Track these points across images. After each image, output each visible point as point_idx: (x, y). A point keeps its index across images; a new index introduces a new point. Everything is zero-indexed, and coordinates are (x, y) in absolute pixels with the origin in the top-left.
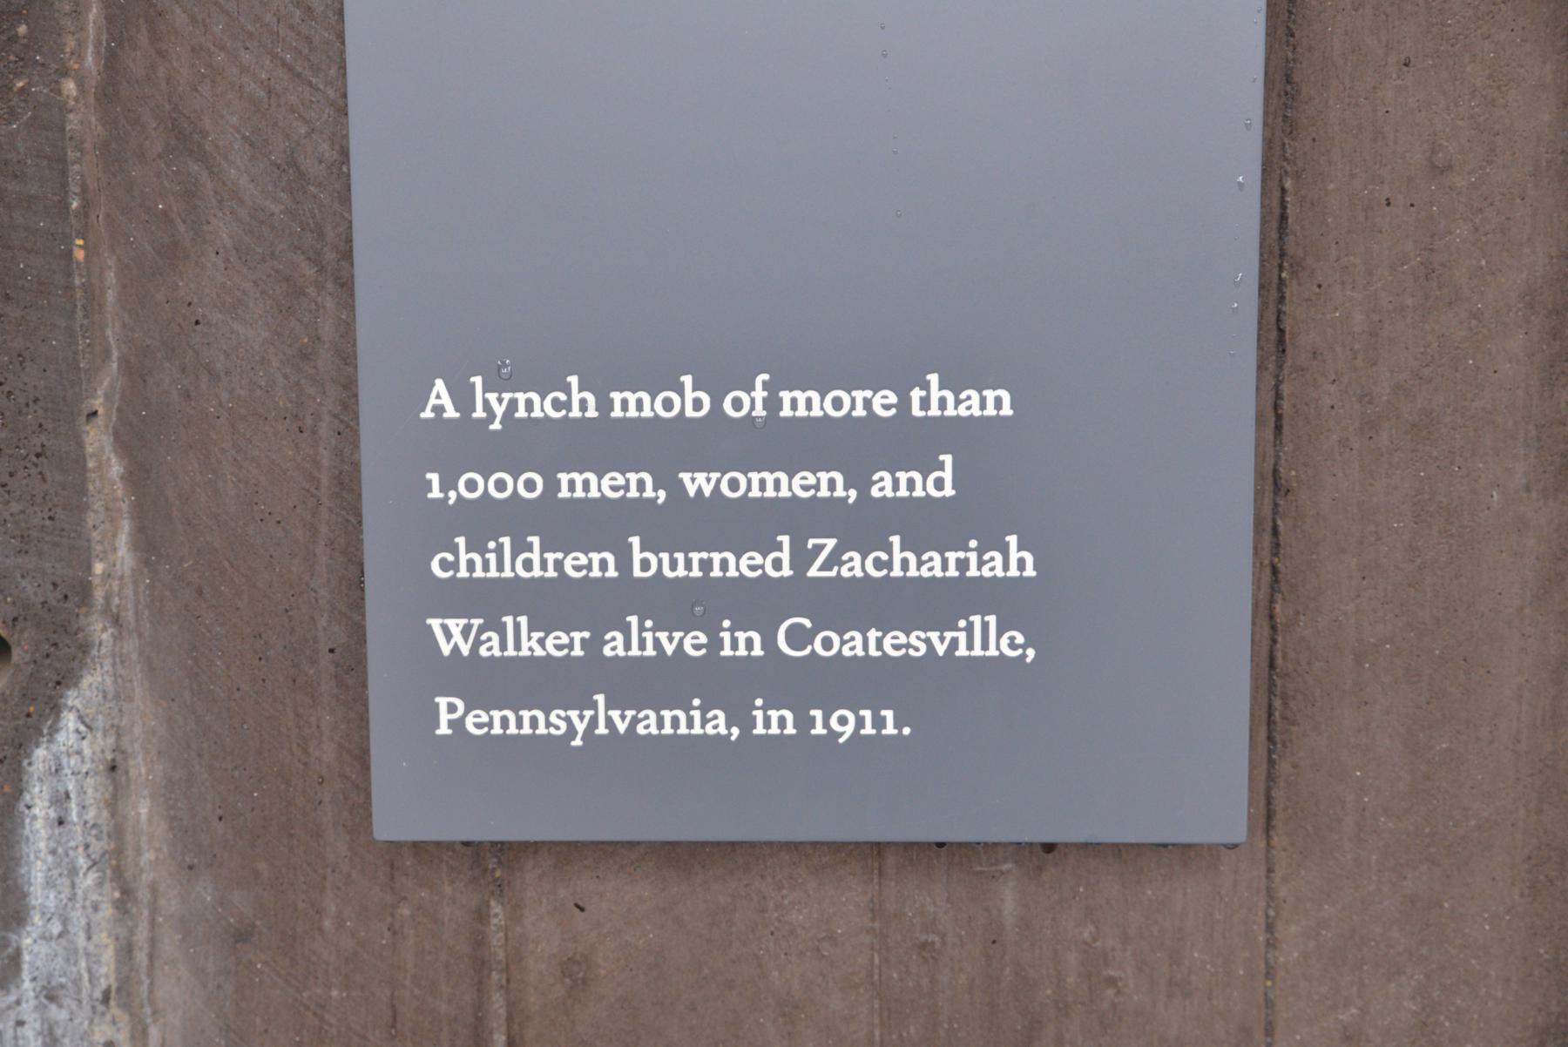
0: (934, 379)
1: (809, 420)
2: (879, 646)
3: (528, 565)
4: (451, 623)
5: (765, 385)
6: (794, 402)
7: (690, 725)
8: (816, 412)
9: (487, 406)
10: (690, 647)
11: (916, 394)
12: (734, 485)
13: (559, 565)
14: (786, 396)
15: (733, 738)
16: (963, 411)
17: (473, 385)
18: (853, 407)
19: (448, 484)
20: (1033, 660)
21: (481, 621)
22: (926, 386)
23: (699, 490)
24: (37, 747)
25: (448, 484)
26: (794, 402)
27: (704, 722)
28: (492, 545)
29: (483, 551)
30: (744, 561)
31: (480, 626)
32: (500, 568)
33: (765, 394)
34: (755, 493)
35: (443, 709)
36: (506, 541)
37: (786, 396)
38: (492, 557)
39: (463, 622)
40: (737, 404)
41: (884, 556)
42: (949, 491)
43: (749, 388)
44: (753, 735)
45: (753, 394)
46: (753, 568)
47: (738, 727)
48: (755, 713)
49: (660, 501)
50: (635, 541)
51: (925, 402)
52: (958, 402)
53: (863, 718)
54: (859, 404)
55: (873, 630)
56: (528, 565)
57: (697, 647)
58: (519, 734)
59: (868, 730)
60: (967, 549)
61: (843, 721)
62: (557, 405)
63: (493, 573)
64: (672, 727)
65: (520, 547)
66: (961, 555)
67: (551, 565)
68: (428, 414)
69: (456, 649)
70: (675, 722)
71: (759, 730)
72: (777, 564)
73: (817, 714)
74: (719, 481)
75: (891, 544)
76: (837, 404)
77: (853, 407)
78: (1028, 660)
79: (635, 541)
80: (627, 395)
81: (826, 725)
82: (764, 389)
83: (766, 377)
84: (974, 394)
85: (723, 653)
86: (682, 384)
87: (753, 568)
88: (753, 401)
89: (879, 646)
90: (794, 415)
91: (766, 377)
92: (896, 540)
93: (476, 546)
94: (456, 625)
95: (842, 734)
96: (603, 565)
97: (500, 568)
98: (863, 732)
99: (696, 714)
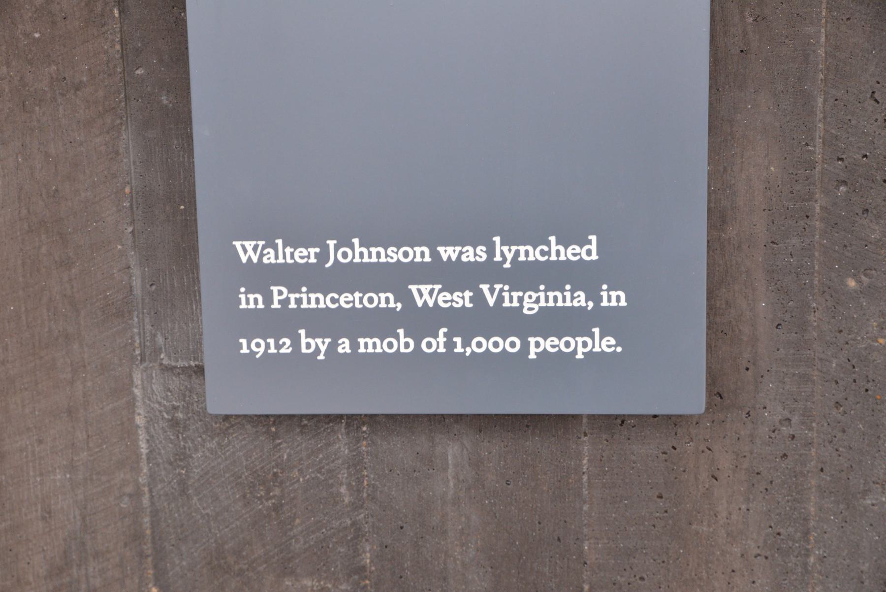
2: (292, 257)
4: (247, 244)
5: (445, 335)
7: (564, 301)
8: (322, 305)
15: (589, 308)
17: (494, 242)
19: (466, 344)
21: (263, 242)
23: (449, 257)
25: (466, 344)
27: (573, 298)
30: (569, 251)
31: (263, 245)
33: (445, 339)
35: (275, 293)
39: (253, 243)
40: (429, 345)
41: (546, 248)
42: (594, 257)
43: (436, 336)
45: (438, 339)
46: (574, 255)
47: (592, 301)
48: (240, 296)
50: (497, 240)
53: (269, 343)
55: (357, 293)
59: (273, 350)
60: (300, 292)
61: (258, 345)
62: (543, 253)
66: (297, 295)
69: (250, 259)
70: (556, 299)
71: (605, 303)
72: (589, 253)
73: (244, 341)
75: (353, 244)
79: (497, 240)
81: (249, 347)
83: (445, 330)
85: (242, 352)
87: (574, 255)
88: (438, 343)
89: (292, 257)
91: (445, 330)
92: (553, 239)
94: (249, 245)
95: (258, 353)
96: (423, 254)
98: (269, 351)
99: (568, 295)
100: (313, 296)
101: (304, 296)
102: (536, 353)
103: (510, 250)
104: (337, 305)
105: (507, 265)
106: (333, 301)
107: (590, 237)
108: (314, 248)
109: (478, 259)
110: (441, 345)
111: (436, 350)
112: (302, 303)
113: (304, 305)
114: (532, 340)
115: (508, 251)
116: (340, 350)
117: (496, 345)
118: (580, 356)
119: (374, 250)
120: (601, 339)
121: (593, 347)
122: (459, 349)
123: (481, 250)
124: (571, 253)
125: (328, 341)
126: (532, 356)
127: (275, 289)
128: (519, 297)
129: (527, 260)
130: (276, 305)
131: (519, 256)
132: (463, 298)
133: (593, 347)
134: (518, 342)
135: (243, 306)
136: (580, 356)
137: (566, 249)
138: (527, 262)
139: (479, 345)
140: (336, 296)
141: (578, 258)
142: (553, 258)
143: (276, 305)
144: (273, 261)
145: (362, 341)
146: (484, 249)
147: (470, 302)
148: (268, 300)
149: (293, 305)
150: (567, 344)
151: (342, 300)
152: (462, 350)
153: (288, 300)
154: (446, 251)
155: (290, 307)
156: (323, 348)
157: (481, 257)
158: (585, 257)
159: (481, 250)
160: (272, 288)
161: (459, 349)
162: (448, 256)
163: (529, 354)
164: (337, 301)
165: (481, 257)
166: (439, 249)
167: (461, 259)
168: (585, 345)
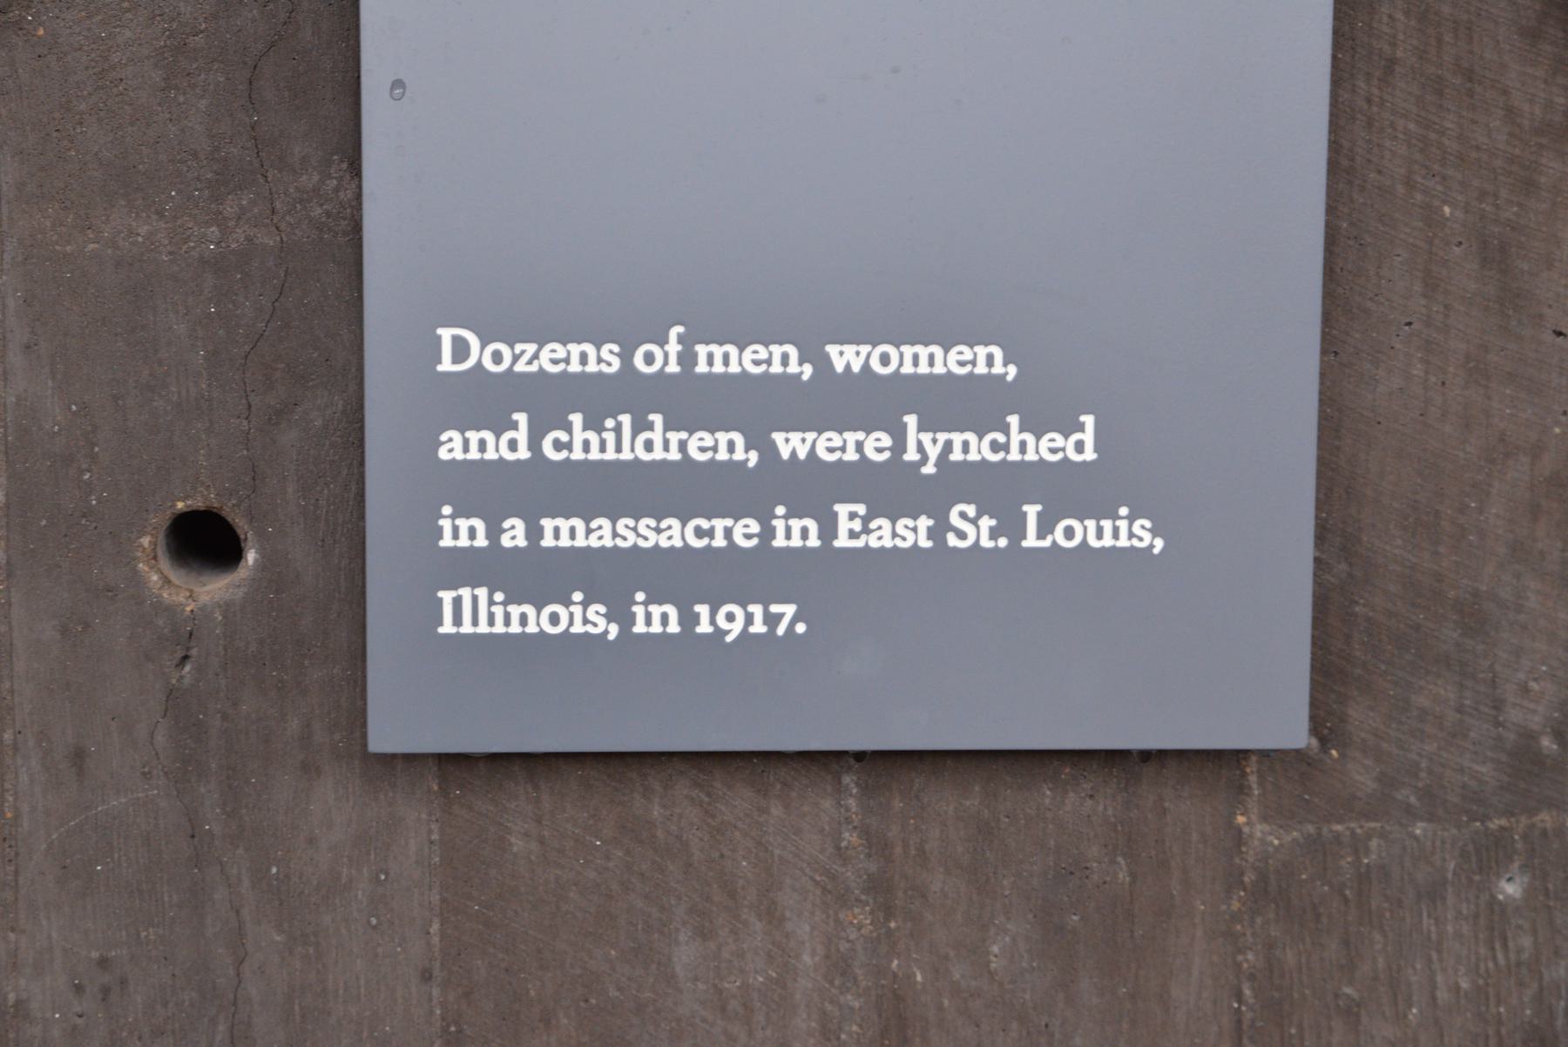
1: (726, 377)
3: (649, 446)
6: (710, 357)
9: (920, 448)
12: (885, 360)
13: (683, 446)
14: (702, 350)
17: (905, 425)
24: (205, 605)
26: (710, 357)
28: (610, 423)
29: (600, 429)
30: (1044, 443)
32: (619, 450)
33: (680, 348)
34: (908, 369)
36: (626, 419)
37: (702, 350)
38: (610, 437)
40: (649, 358)
41: (1001, 438)
42: (1089, 455)
43: (662, 342)
44: (1021, 547)
45: (667, 348)
46: (1053, 451)
48: (441, 522)
50: (911, 421)
52: (589, 531)
56: (649, 446)
57: (748, 537)
58: (523, 632)
59: (758, 627)
61: (730, 617)
63: (610, 455)
65: (641, 425)
67: (674, 446)
71: (640, 628)
72: (1080, 447)
75: (1008, 425)
79: (911, 421)
81: (713, 622)
83: (680, 329)
85: (441, 630)
87: (1053, 451)
88: (666, 355)
91: (680, 329)
92: (1014, 420)
93: (594, 424)
95: (728, 632)
97: (619, 450)
98: (752, 630)
103: (935, 441)
105: (929, 469)
107: (1083, 418)
108: (855, 431)
110: (673, 359)
111: (567, 630)
115: (931, 444)
119: (474, 437)
124: (1047, 448)
127: (842, 510)
131: (951, 451)
132: (915, 530)
135: (447, 541)
137: (1038, 439)
138: (965, 464)
141: (1059, 456)
142: (1014, 456)
144: (459, 455)
147: (929, 538)
154: (787, 440)
158: (1074, 457)
160: (440, 331)
162: (791, 449)
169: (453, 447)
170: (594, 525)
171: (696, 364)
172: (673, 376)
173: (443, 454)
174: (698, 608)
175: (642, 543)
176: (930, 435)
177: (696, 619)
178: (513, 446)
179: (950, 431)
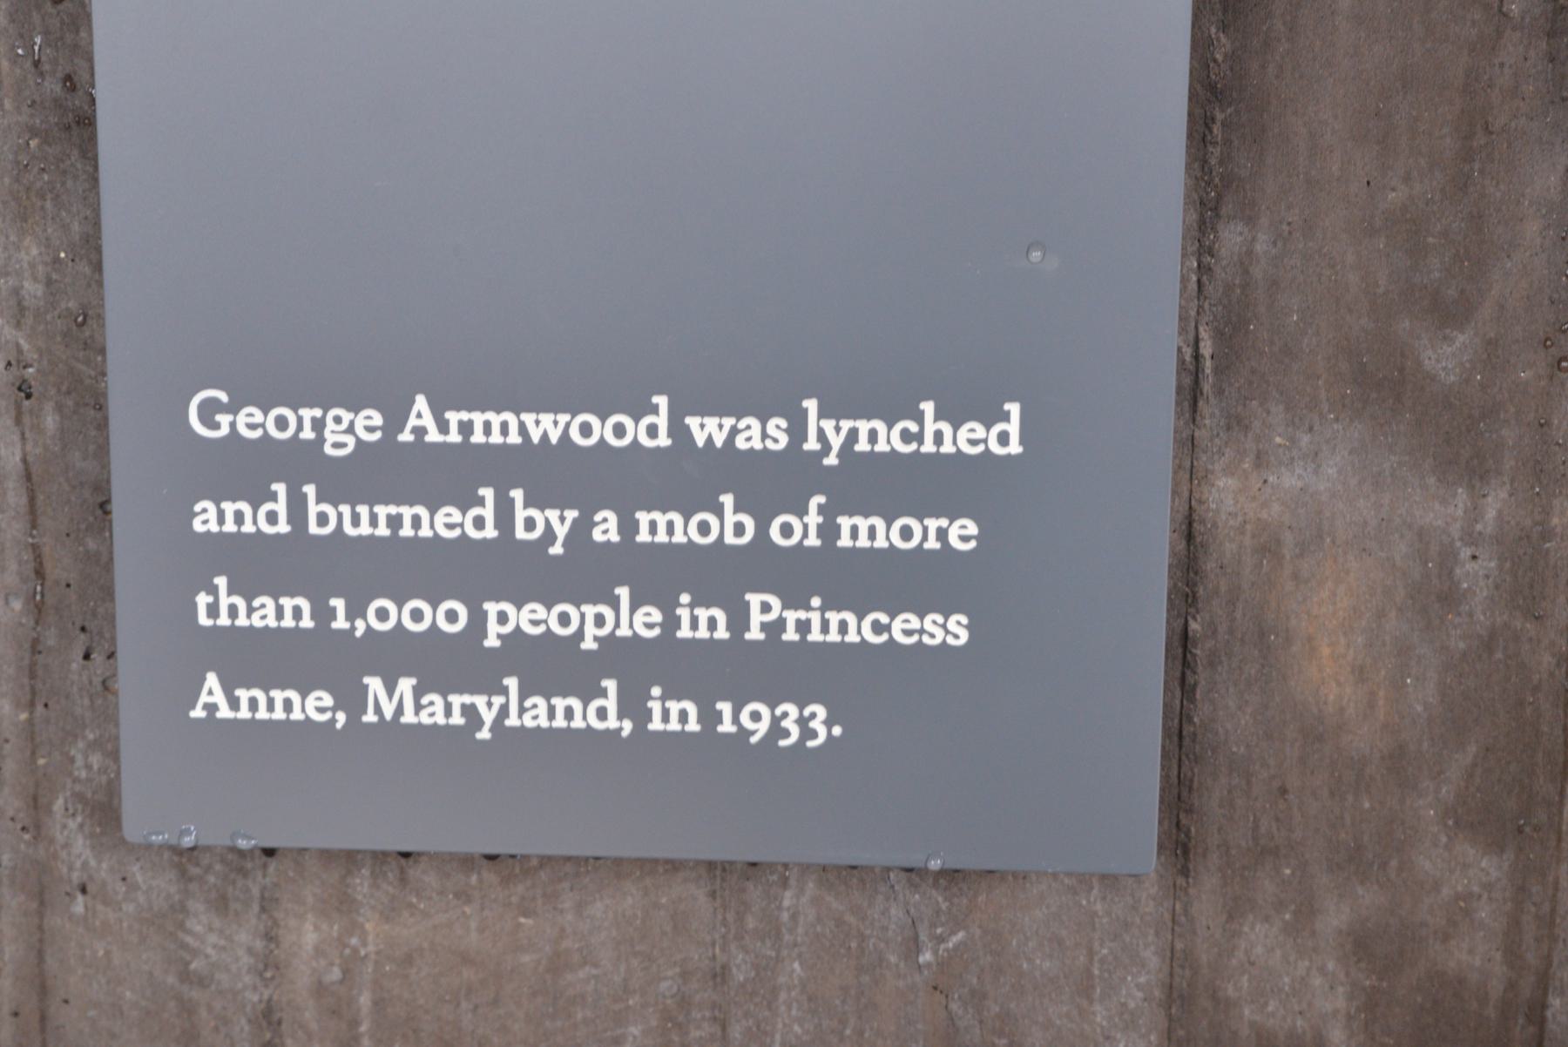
0: (221, 582)
5: (821, 509)
10: (314, 710)
11: (203, 600)
14: (845, 522)
16: (257, 622)
17: (305, 495)
18: (925, 538)
19: (356, 611)
20: (344, 727)
22: (213, 591)
23: (710, 440)
25: (356, 611)
30: (963, 434)
33: (820, 520)
37: (845, 522)
40: (787, 530)
41: (913, 427)
42: (1015, 448)
43: (802, 512)
45: (806, 519)
46: (450, 526)
48: (650, 704)
49: (625, 733)
50: (811, 405)
51: (213, 611)
52: (250, 611)
54: (932, 534)
60: (808, 608)
61: (756, 717)
62: (906, 436)
64: (680, 721)
66: (802, 615)
68: (406, 437)
71: (656, 725)
72: (1004, 439)
74: (568, 425)
76: (906, 533)
77: (925, 538)
78: (339, 726)
79: (811, 405)
80: (656, 515)
81: (736, 720)
82: (819, 513)
84: (268, 601)
85: (720, 729)
86: (722, 505)
88: (806, 527)
90: (872, 546)
92: (928, 407)
95: (753, 733)
100: (834, 617)
101: (815, 618)
102: (499, 636)
104: (884, 637)
105: (831, 460)
106: (878, 628)
107: (1007, 407)
109: (770, 444)
110: (812, 531)
112: (809, 631)
113: (815, 636)
114: (492, 608)
116: (597, 535)
117: (417, 615)
118: (588, 644)
120: (633, 610)
121: (617, 625)
122: (340, 623)
123: (778, 427)
124: (967, 438)
125: (370, 717)
126: (492, 642)
128: (314, 420)
129: (253, 717)
130: (755, 634)
133: (617, 625)
134: (462, 611)
136: (588, 644)
137: (956, 428)
139: (382, 615)
140: (884, 618)
142: (928, 447)
143: (755, 634)
145: (643, 518)
146: (784, 424)
148: (739, 620)
149: (791, 635)
150: (564, 619)
151: (897, 626)
152: (347, 625)
153: (780, 624)
154: (702, 426)
155: (785, 637)
156: (561, 531)
157: (776, 441)
159: (778, 427)
160: (748, 597)
161: (340, 623)
163: (485, 636)
164: (888, 628)
165: (776, 441)
166: (689, 420)
167: (734, 442)
168: (600, 621)
169: (206, 518)
170: (256, 603)
171: (839, 537)
172: (812, 549)
173: (198, 526)
174: (720, 706)
175: (951, 640)
176: (832, 423)
177: (718, 718)
178: (272, 518)
179: (855, 418)
